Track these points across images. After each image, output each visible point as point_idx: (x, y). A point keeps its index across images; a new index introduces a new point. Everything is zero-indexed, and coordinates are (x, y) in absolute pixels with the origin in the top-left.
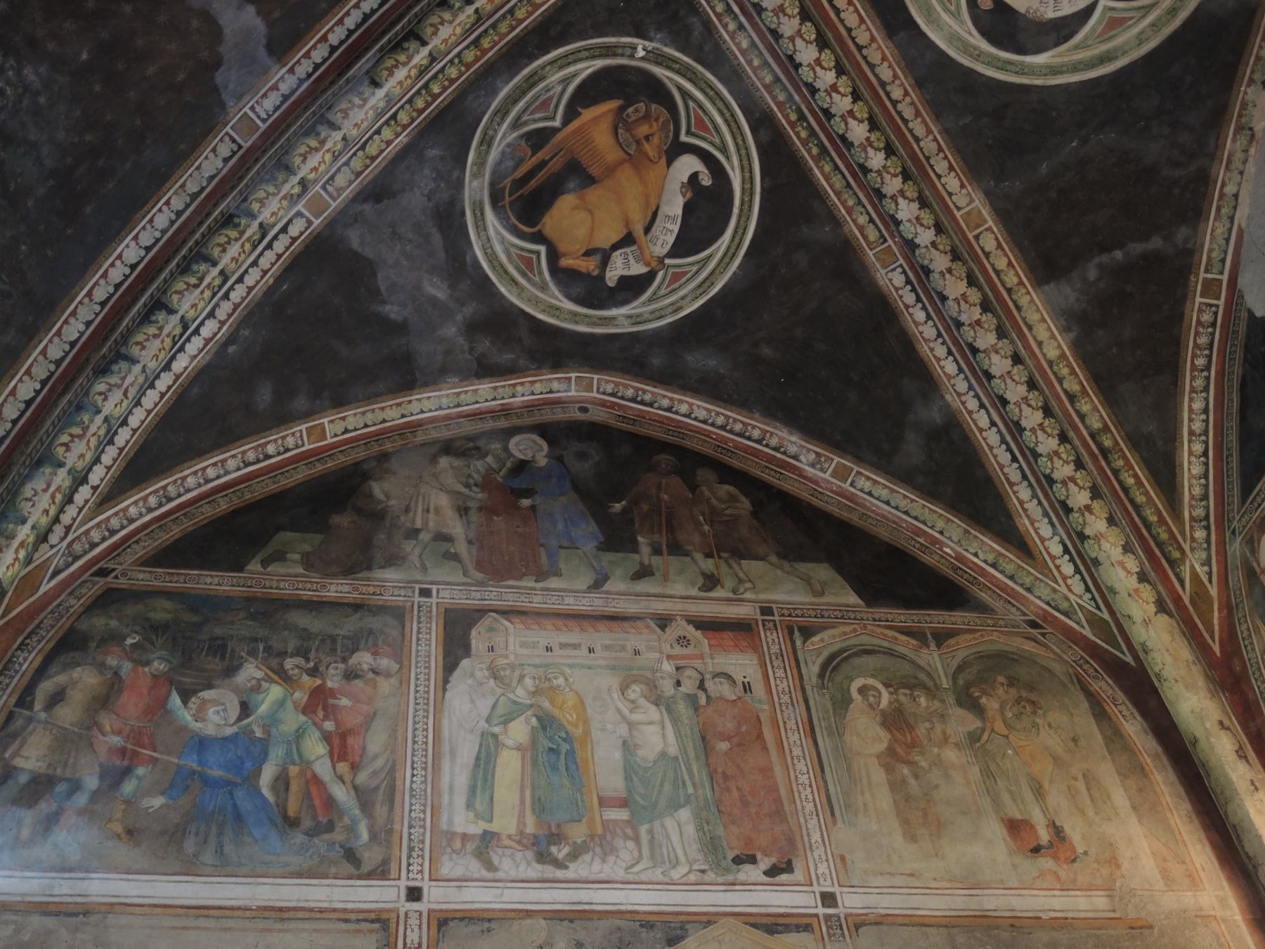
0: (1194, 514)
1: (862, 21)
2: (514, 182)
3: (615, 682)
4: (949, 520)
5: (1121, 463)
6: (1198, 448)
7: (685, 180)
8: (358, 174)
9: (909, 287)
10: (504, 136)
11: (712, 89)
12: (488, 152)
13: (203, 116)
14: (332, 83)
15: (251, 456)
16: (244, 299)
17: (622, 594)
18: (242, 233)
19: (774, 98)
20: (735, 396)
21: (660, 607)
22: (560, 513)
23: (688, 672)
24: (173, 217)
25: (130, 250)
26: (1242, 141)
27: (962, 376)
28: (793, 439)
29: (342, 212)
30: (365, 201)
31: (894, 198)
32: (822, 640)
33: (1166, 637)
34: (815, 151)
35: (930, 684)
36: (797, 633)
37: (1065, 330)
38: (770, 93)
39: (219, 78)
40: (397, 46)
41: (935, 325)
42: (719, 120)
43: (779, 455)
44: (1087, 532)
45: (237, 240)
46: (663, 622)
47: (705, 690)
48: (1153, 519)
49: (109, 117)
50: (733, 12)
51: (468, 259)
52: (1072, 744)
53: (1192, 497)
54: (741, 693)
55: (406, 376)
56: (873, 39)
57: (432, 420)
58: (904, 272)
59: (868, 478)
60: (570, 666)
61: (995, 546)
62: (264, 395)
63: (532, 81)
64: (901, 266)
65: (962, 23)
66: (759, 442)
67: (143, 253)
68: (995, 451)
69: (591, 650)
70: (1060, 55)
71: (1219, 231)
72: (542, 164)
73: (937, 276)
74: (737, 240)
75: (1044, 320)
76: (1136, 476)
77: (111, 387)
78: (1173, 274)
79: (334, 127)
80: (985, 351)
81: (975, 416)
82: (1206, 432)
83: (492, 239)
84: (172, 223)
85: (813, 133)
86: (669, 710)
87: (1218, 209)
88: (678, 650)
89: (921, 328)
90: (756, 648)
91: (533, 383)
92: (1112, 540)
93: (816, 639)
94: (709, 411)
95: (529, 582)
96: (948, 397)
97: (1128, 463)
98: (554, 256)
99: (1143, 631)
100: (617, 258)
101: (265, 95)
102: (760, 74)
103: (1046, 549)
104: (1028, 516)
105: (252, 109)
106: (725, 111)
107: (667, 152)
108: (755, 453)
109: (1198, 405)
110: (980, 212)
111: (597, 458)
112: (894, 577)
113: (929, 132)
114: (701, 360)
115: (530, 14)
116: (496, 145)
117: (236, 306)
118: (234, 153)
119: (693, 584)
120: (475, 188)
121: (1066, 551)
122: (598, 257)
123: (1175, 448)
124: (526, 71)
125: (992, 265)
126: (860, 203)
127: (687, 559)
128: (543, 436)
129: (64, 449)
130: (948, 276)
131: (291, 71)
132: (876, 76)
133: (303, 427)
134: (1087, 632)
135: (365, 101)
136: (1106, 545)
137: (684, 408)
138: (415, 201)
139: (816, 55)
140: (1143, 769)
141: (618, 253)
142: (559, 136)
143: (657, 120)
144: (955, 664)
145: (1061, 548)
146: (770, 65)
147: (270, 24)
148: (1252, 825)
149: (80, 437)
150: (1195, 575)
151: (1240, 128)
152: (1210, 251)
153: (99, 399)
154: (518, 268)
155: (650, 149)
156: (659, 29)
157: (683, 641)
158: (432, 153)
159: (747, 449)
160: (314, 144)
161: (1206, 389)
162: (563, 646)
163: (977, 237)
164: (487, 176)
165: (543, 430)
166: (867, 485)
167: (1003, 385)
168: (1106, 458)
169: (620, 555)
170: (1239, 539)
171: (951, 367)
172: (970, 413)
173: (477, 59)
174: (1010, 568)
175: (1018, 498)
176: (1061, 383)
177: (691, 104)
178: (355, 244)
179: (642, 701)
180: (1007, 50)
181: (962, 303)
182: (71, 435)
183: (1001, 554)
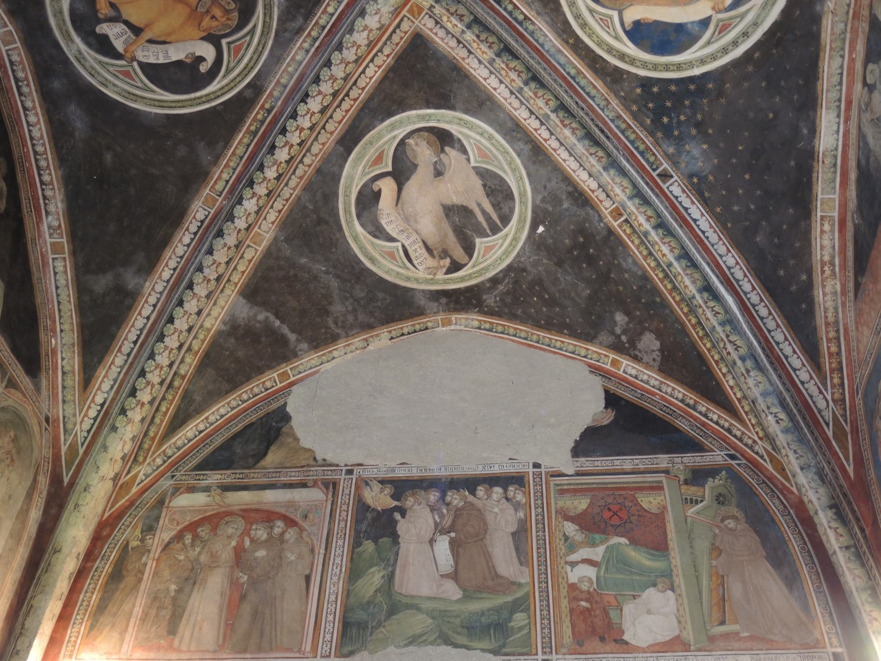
0: (167, 451)
1: (340, 122)
4: (73, 330)
5: (170, 397)
6: (201, 427)
7: (197, 54)
9: (199, 224)
11: (263, 48)
19: (273, 89)
20: (64, 151)
27: (165, 284)
28: (59, 205)
31: (254, 194)
34: (253, 128)
37: (224, 323)
38: (276, 85)
41: (186, 252)
42: (245, 60)
43: (41, 201)
44: (129, 413)
48: (151, 434)
50: (315, 42)
52: (7, 498)
53: (175, 443)
56: (332, 133)
58: (207, 217)
59: (65, 266)
64: (209, 213)
65: (361, 179)
66: (42, 183)
68: (133, 329)
70: (365, 237)
71: (313, 362)
74: (173, 105)
75: (223, 308)
76: (168, 409)
78: (278, 352)
80: (194, 294)
81: (146, 305)
82: (211, 424)
85: (262, 122)
87: (324, 354)
89: (179, 245)
92: (134, 428)
94: (42, 137)
96: (147, 284)
97: (172, 401)
99: (96, 481)
100: (120, 28)
102: (286, 74)
103: (95, 394)
104: (107, 371)
106: (253, 62)
107: (209, 34)
108: (33, 185)
109: (222, 411)
110: (263, 240)
113: (294, 189)
114: (77, 118)
121: (102, 405)
122: (111, 13)
123: (195, 416)
125: (238, 263)
126: (235, 169)
130: (226, 249)
134: (64, 449)
136: (129, 428)
137: (32, 119)
139: (316, 111)
140: (20, 539)
143: (228, 19)
145: (101, 401)
146: (291, 78)
148: (43, 614)
150: (136, 475)
151: (366, 340)
152: (302, 364)
155: (206, 22)
161: (233, 409)
163: (249, 246)
166: (60, 268)
167: (181, 315)
170: (172, 482)
171: (166, 275)
172: (146, 301)
175: (114, 359)
176: (194, 339)
177: (248, 38)
180: (356, 209)
181: (215, 265)
183: (73, 372)
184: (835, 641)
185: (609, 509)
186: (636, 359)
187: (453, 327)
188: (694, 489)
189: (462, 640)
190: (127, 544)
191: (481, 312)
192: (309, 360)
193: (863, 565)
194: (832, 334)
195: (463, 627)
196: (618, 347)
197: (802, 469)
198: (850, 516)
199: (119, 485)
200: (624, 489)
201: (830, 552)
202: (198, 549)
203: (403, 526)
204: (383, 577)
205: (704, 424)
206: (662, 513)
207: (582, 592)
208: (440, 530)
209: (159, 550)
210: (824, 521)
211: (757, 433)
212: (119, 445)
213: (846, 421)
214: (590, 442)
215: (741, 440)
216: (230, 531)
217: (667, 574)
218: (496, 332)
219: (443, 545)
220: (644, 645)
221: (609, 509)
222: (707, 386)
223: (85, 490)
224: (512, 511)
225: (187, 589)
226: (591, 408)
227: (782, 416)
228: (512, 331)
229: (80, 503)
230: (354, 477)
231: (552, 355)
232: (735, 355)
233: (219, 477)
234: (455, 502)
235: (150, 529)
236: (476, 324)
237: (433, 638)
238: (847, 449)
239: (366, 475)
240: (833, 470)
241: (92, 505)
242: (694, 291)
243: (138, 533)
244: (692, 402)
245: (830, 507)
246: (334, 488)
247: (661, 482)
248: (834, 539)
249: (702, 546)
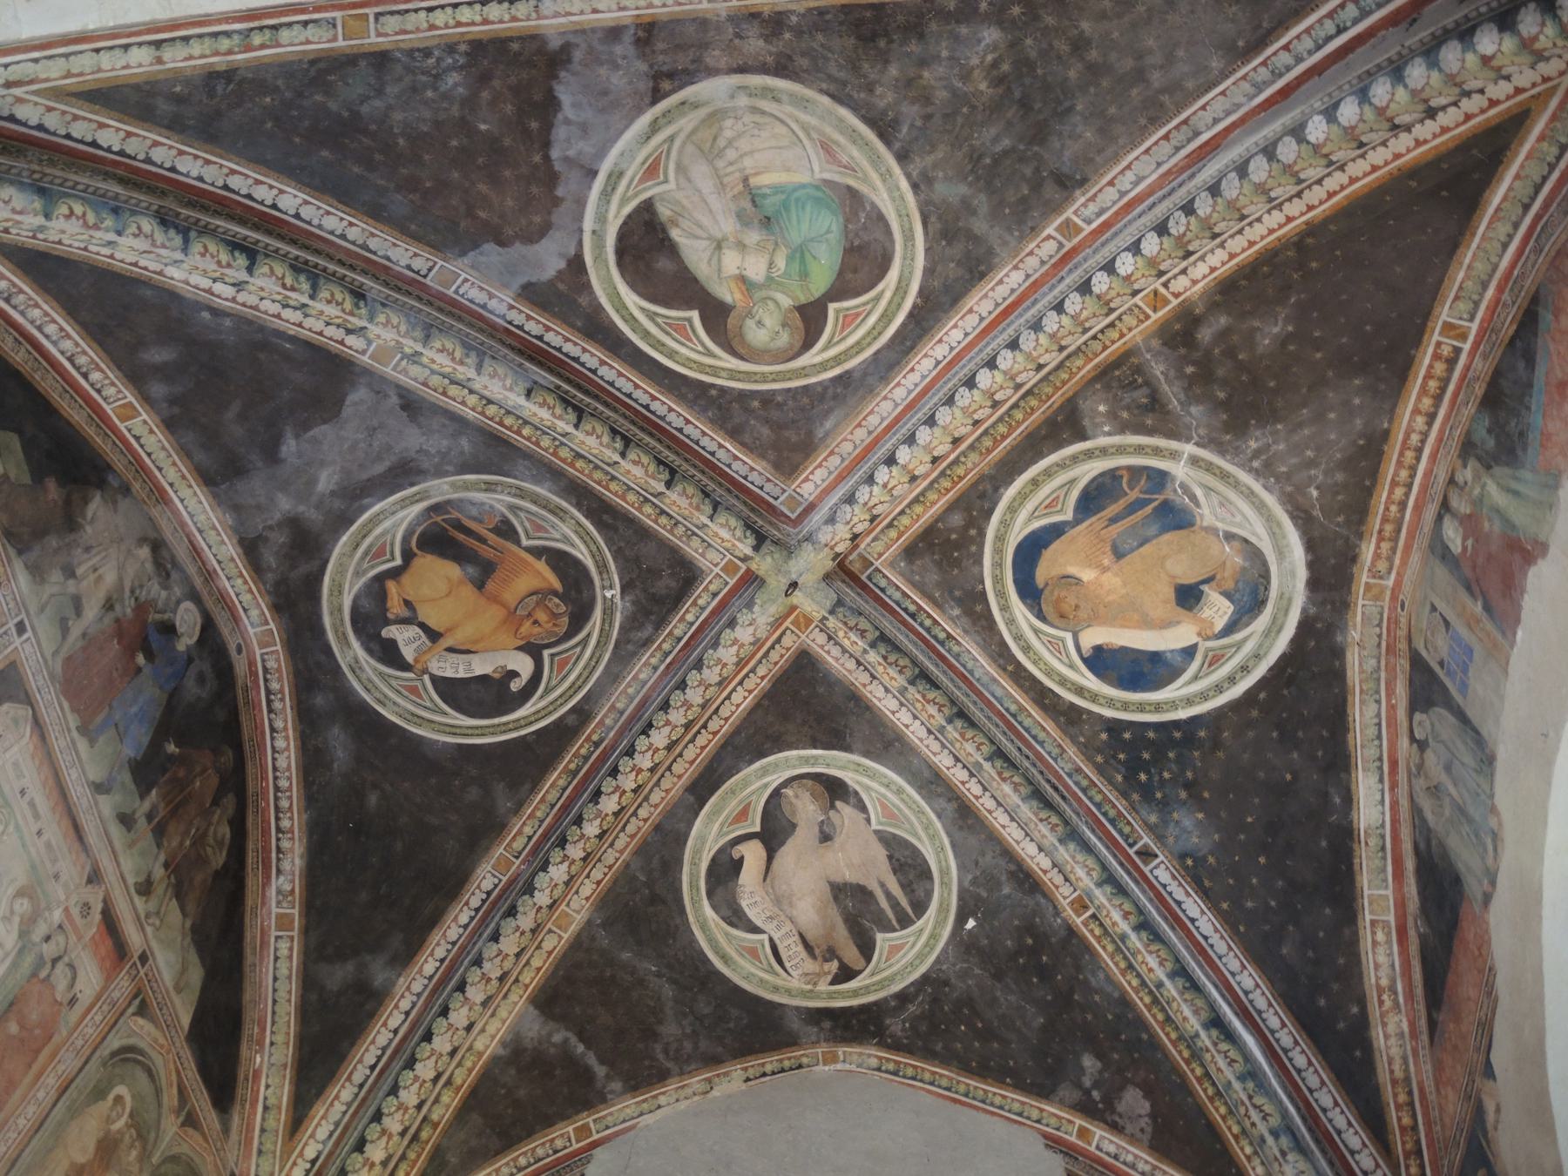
1: (692, 763)
2: (458, 520)
3: (22, 880)
8: (425, 384)
10: (499, 502)
12: (480, 490)
13: (451, 236)
14: (513, 348)
15: (82, 360)
16: (266, 313)
17: (98, 813)
18: (352, 314)
19: (605, 716)
21: (106, 864)
22: (142, 699)
23: (61, 939)
24: (338, 232)
25: (291, 200)
26: (701, 1087)
28: (298, 861)
29: (383, 379)
30: (401, 396)
32: (142, 1027)
34: (572, 766)
35: (149, 1147)
36: (137, 1002)
37: (503, 1044)
38: (609, 710)
39: (489, 247)
40: (566, 402)
43: (274, 855)
45: (343, 311)
46: (94, 877)
47: (53, 967)
49: (427, 157)
51: (366, 501)
54: (65, 1002)
55: (220, 473)
56: (680, 777)
57: (176, 512)
59: (291, 949)
60: (17, 827)
61: (285, 1099)
62: (159, 355)
63: (557, 511)
65: (716, 841)
66: (279, 830)
67: (292, 212)
69: (39, 833)
70: (717, 925)
71: (628, 1111)
72: (482, 540)
73: (513, 924)
77: (150, 237)
79: (479, 368)
83: (394, 517)
84: (332, 233)
85: (586, 758)
86: (21, 952)
87: (644, 1101)
88: (75, 912)
90: (109, 979)
91: (250, 591)
93: (141, 1021)
94: (289, 768)
95: (73, 721)
96: (402, 979)
97: (415, 1162)
98: (395, 573)
101: (482, 289)
105: (466, 280)
107: (529, 643)
108: (266, 832)
111: (204, 695)
112: (218, 1038)
113: (621, 852)
115: (616, 494)
116: (486, 497)
117: (255, 308)
118: (418, 273)
119: (137, 874)
120: (441, 488)
121: (313, 1162)
122: (405, 613)
124: (564, 504)
126: (542, 822)
127: (155, 850)
128: (204, 629)
129: (67, 212)
131: (511, 307)
132: (651, 790)
133: (131, 398)
135: (511, 389)
137: (280, 744)
138: (412, 440)
141: (418, 630)
142: (514, 548)
144: (176, 1150)
147: (551, 283)
149: (86, 225)
151: (709, 1080)
153: (133, 229)
154: (370, 546)
155: (526, 627)
156: (633, 603)
157: (86, 908)
158: (464, 443)
159: (267, 822)
160: (458, 354)
162: (32, 804)
163: (550, 931)
164: (456, 496)
165: (208, 625)
166: (284, 952)
168: (411, 1142)
169: (133, 787)
171: (429, 968)
172: (396, 1006)
173: (564, 461)
177: (578, 650)
178: (352, 398)
179: (17, 919)
182: (84, 214)
183: (279, 1108)
186: (1116, 1128)
187: (839, 1066)
191: (882, 1045)
192: (622, 1108)
194: (1402, 1098)
196: (1086, 1108)
228: (927, 1076)
232: (1262, 1128)
236: (874, 1062)
242: (1197, 1027)
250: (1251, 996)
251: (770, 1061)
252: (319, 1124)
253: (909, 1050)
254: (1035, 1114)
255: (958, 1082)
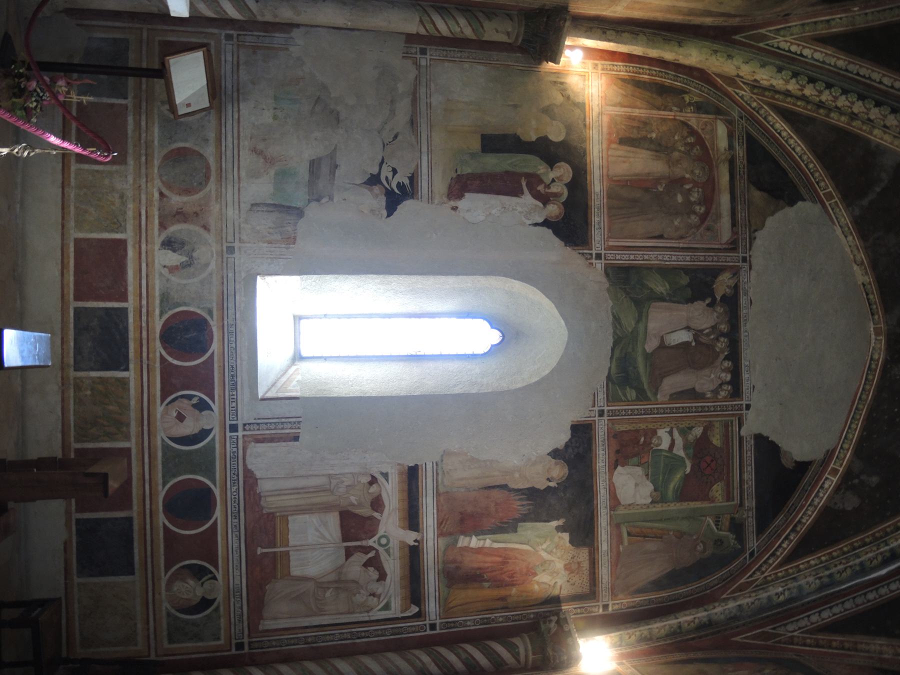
5: (809, 107)
6: (784, 134)
26: (858, 258)
33: (726, 70)
37: (878, 145)
48: (777, 96)
53: (770, 115)
76: (799, 106)
78: (849, 195)
82: (786, 141)
84: (830, 617)
97: (807, 109)
99: (736, 63)
104: (831, 55)
109: (798, 149)
121: (801, 55)
134: (763, 31)
136: (781, 82)
151: (862, 263)
174: (820, 26)
184: (616, 607)
185: (712, 461)
186: (837, 489)
187: (873, 336)
188: (727, 524)
189: (617, 353)
190: (686, 93)
191: (886, 363)
192: (845, 217)
193: (667, 636)
194: (847, 645)
195: (626, 354)
196: (848, 475)
197: (739, 606)
198: (703, 633)
199: (731, 80)
200: (728, 473)
201: (677, 615)
202: (683, 149)
203: (700, 305)
204: (662, 293)
205: (779, 536)
206: (709, 500)
207: (651, 438)
208: (698, 334)
209: (682, 119)
210: (699, 615)
211: (770, 576)
212: (766, 76)
213: (776, 642)
214: (766, 449)
215: (765, 562)
216: (697, 172)
217: (663, 500)
218: (867, 374)
219: (684, 337)
220: (615, 478)
221: (712, 461)
222: (809, 544)
223: (729, 56)
224: (712, 387)
225: (652, 146)
226: (797, 448)
227: (782, 598)
228: (868, 387)
229: (718, 54)
230: (740, 264)
231: (844, 420)
232: (834, 570)
233: (741, 155)
234: (719, 345)
235: (699, 108)
236: (876, 357)
237: (618, 332)
238: (754, 639)
239: (742, 273)
240: (737, 627)
241: (717, 63)
242: (892, 546)
243: (696, 99)
244: (798, 529)
245: (710, 621)
246: (731, 249)
247: (733, 500)
248: (686, 619)
249: (684, 526)
250: (806, 619)
251: (875, 297)
252: (822, 52)
253: (883, 377)
254: (846, 446)
255: (864, 405)
